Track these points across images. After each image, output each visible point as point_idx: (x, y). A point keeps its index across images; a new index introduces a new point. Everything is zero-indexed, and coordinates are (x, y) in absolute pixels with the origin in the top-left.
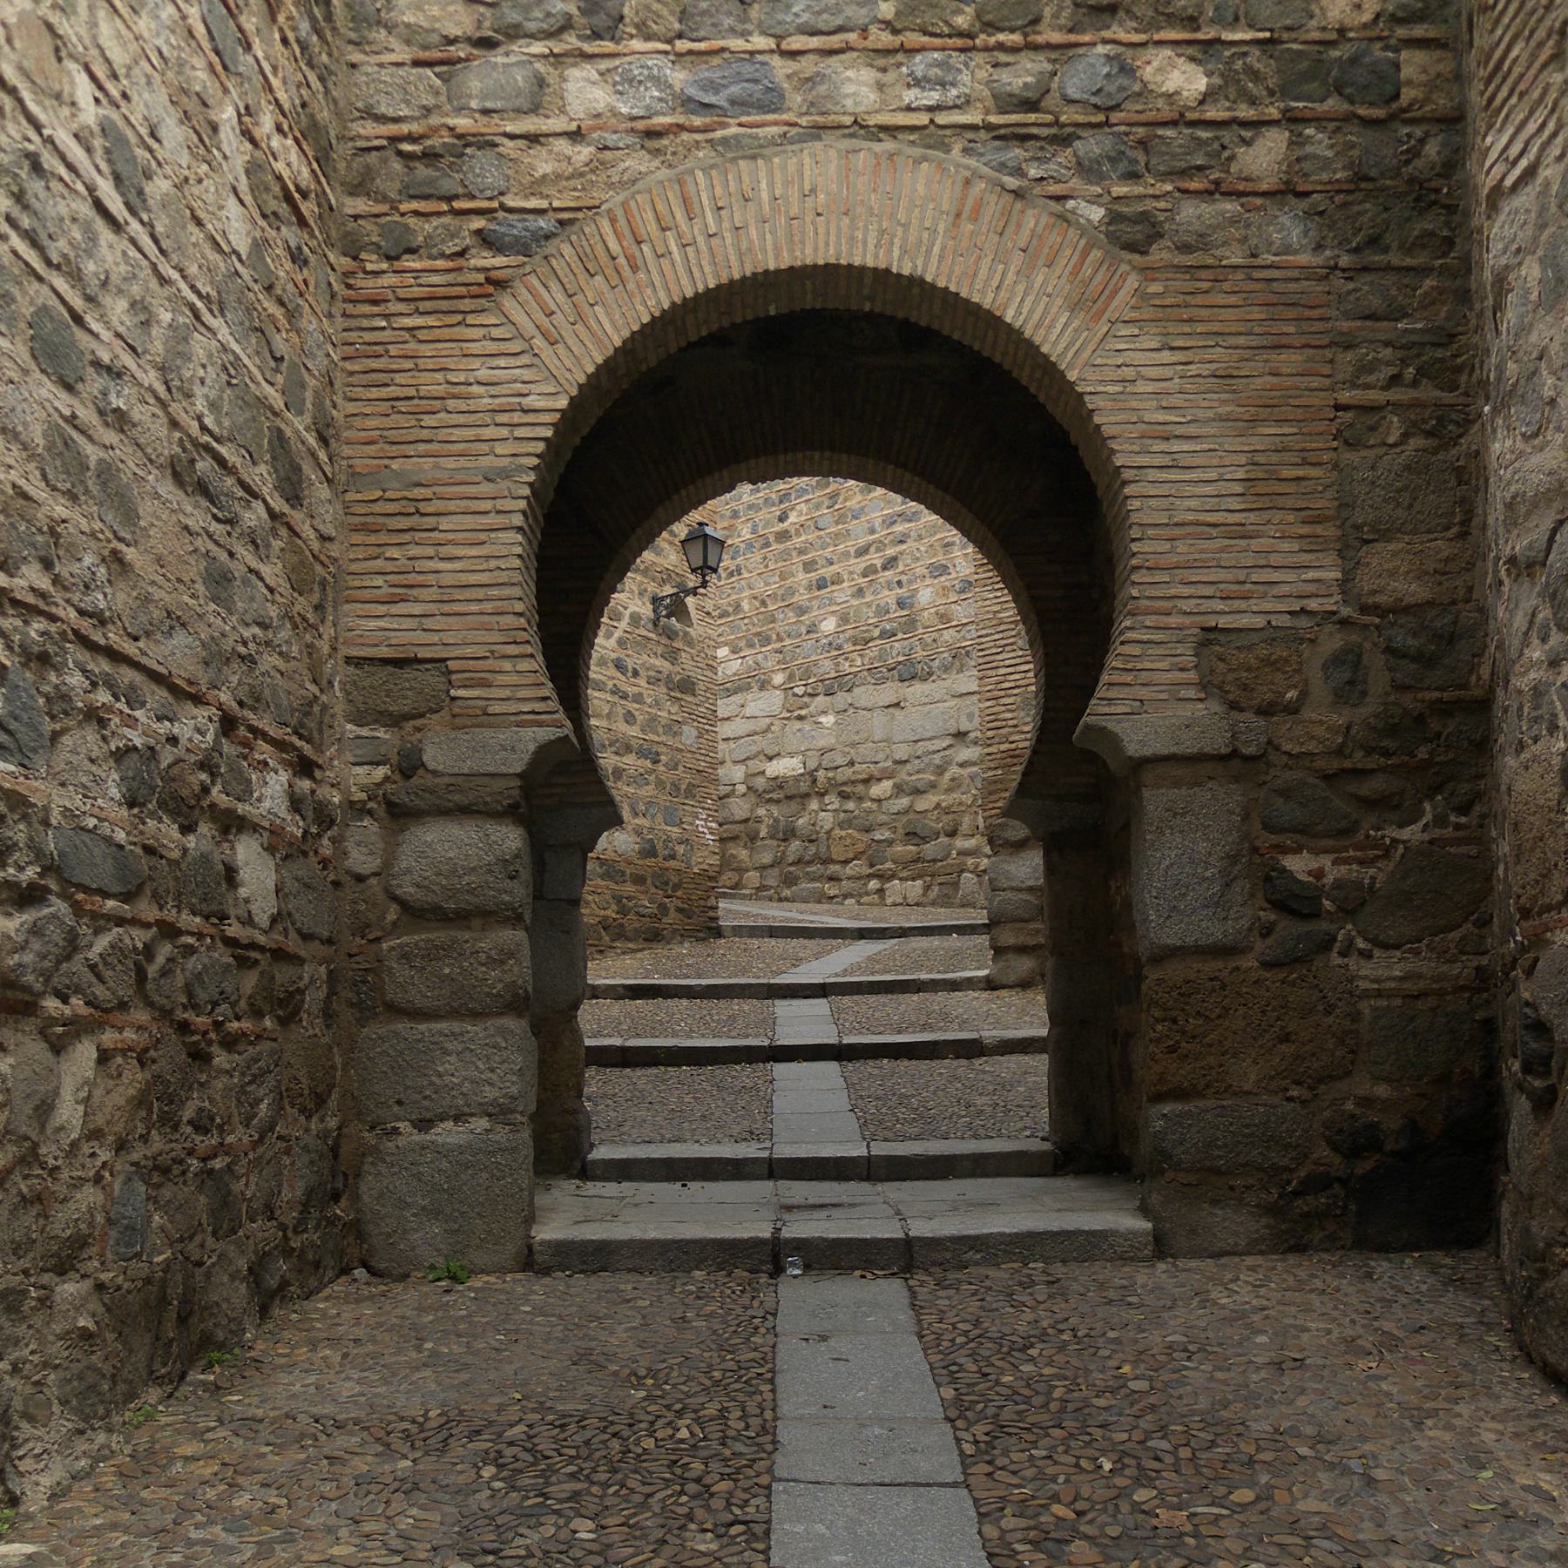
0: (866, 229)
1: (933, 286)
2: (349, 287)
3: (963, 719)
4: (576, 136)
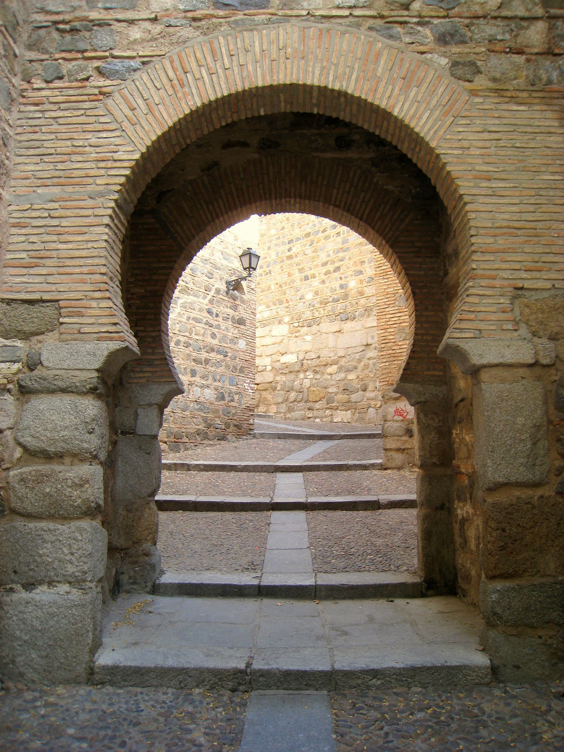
0: (314, 67)
1: (352, 96)
2: (24, 97)
3: (370, 338)
4: (155, 20)
